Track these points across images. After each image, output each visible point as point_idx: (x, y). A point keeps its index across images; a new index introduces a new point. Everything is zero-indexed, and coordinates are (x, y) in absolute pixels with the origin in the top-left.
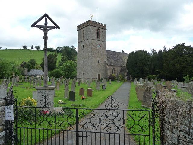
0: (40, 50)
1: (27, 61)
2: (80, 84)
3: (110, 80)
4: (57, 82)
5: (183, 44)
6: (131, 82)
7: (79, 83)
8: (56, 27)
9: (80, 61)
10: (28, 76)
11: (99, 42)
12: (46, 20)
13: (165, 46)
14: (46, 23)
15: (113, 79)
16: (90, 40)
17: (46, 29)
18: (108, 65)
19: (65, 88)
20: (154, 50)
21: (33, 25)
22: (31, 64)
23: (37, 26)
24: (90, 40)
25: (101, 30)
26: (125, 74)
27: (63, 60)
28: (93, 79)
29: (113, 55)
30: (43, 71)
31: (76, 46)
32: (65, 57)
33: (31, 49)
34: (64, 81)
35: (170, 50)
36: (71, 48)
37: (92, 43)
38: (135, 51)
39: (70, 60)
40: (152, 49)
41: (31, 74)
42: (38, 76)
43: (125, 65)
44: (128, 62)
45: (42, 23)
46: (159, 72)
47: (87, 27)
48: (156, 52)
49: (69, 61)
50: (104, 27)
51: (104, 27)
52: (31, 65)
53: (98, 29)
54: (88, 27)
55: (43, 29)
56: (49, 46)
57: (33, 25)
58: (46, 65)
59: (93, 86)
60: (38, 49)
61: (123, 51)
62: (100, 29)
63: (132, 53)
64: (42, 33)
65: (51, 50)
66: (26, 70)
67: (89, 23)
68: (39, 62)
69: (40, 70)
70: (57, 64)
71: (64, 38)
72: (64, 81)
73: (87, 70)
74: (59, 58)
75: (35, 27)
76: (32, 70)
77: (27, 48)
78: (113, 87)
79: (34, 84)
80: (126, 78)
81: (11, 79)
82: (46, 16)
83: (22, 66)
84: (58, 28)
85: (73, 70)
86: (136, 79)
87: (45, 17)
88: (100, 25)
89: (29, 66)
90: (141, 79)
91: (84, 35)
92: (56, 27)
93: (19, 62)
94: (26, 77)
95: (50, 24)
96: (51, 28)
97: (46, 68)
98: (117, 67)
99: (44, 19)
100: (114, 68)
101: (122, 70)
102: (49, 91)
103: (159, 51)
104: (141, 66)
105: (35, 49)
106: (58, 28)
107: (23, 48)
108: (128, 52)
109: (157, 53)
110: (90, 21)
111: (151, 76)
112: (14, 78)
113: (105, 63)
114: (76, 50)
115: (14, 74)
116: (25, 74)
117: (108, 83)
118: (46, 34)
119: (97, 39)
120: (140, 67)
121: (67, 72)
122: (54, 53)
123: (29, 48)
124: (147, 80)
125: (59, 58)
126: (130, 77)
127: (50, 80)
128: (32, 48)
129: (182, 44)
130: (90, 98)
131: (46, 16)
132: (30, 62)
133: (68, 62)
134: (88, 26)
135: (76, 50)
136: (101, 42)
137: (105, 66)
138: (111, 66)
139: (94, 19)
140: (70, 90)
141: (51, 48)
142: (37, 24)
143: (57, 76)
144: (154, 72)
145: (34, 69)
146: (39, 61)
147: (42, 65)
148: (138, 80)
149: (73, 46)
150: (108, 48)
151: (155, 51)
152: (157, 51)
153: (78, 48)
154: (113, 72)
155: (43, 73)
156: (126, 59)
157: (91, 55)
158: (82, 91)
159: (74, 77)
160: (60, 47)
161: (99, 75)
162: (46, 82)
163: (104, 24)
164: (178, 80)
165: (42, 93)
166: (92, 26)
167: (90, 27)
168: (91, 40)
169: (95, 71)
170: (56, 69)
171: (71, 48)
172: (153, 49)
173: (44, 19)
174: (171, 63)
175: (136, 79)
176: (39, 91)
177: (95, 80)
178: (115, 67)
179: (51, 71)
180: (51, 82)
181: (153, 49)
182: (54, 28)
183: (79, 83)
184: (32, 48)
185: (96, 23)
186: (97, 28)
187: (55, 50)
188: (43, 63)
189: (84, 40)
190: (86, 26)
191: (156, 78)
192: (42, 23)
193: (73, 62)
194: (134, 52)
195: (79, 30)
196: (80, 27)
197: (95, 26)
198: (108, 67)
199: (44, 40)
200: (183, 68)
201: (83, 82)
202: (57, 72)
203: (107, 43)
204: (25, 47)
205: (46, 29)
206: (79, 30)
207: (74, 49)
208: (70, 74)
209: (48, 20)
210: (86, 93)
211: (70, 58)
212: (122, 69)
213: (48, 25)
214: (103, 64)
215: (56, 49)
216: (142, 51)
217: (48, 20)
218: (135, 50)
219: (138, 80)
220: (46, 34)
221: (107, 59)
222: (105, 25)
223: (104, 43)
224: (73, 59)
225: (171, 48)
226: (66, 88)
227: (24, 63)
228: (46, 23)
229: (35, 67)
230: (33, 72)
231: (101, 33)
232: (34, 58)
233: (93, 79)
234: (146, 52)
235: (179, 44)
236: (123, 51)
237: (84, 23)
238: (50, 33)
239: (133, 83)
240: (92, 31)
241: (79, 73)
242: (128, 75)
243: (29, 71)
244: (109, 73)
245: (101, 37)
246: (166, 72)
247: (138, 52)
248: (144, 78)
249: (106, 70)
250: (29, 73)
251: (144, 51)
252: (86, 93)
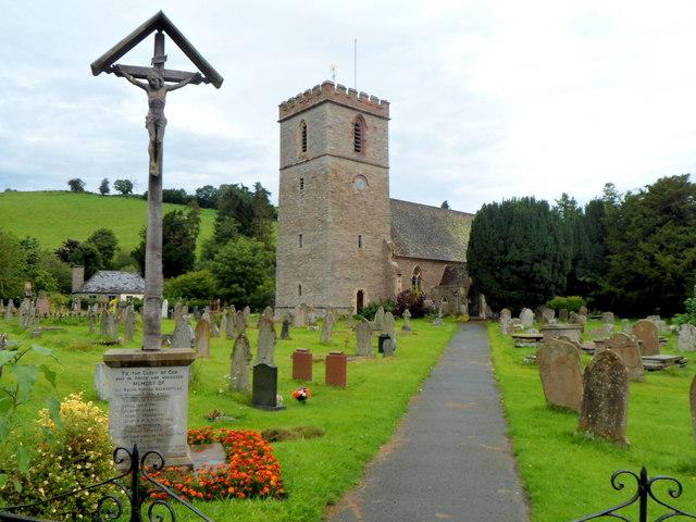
0: (136, 197)
1: (82, 238)
2: (290, 329)
3: (407, 313)
4: (201, 323)
5: (686, 177)
6: (483, 323)
7: (286, 326)
8: (203, 76)
9: (283, 238)
10: (87, 297)
11: (361, 169)
12: (159, 41)
13: (608, 185)
14: (159, 59)
15: (419, 312)
16: (328, 161)
17: (156, 82)
18: (396, 258)
19: (234, 349)
20: (570, 199)
21: (104, 65)
22: (100, 250)
23: (119, 72)
24: (328, 161)
25: (368, 120)
26: (462, 291)
27: (222, 238)
28: (339, 311)
29: (427, 221)
30: (143, 276)
31: (272, 185)
32: (231, 224)
33: (99, 192)
34: (224, 317)
35: (631, 200)
36: (252, 190)
37: (334, 171)
38: (499, 202)
39: (249, 235)
40: (559, 198)
41: (98, 287)
42: (123, 297)
43: (459, 255)
44: (471, 244)
45: (141, 56)
46: (595, 286)
47: (315, 110)
48: (578, 206)
49: (242, 241)
50: (380, 111)
51: (380, 111)
52: (94, 256)
53: (360, 118)
54: (320, 108)
55: (145, 82)
56: (169, 182)
57: (104, 65)
58: (154, 248)
59: (343, 338)
60: (125, 193)
61: (445, 205)
62: (365, 116)
63: (489, 212)
64: (139, 99)
65: (174, 197)
66: (78, 273)
67: (323, 97)
68: (129, 244)
69: (131, 272)
70: (198, 252)
71: (227, 141)
72: (224, 317)
73: (319, 278)
74: (207, 226)
75: (108, 72)
76: (102, 273)
77: (86, 189)
78: (419, 341)
79: (105, 325)
80: (464, 308)
81: (17, 304)
82: (160, 24)
83: (63, 256)
84: (213, 78)
85: (259, 276)
86: (506, 313)
87: (156, 31)
88: (367, 103)
89: (93, 255)
90: (528, 313)
91: (305, 140)
92: (203, 76)
93: (50, 243)
94: (77, 298)
95: (177, 61)
96: (181, 79)
97: (154, 262)
98: (429, 264)
99: (152, 37)
100: (417, 270)
101: (448, 278)
102: (167, 369)
103: (593, 203)
104: (519, 262)
105: (113, 191)
106: (213, 78)
107: (69, 188)
108: (469, 202)
109: (580, 209)
110: (328, 85)
111: (563, 300)
112: (26, 304)
113: (387, 248)
114: (274, 200)
115: (28, 286)
116: (74, 290)
117: (400, 323)
118: (156, 106)
119: (355, 156)
120: (520, 263)
121: (235, 286)
122: (186, 211)
123: (92, 187)
124: (549, 314)
125: (207, 226)
126: (479, 302)
127: (169, 314)
128: (104, 188)
129: (679, 174)
130: (333, 391)
131: (160, 24)
132: (94, 239)
133: (242, 245)
134: (320, 104)
135: (269, 198)
136: (368, 167)
137: (385, 261)
138: (405, 262)
139: (345, 79)
140: (254, 362)
141: (178, 188)
142: (122, 61)
143: (197, 297)
144: (574, 287)
145: (109, 268)
146: (127, 242)
147: (139, 258)
148: (516, 314)
149: (258, 185)
150: (393, 195)
151: (573, 202)
152: (582, 203)
153: (282, 190)
154: (414, 283)
155: (142, 283)
156: (463, 236)
157: (330, 219)
158: (302, 362)
159: (262, 303)
160: (208, 188)
161: (360, 295)
162: (152, 328)
163: (381, 97)
164: (667, 314)
165: (132, 380)
166: (336, 106)
167: (328, 106)
168: (334, 160)
169: (347, 279)
170: (192, 269)
171: (252, 190)
172: (565, 196)
173: (152, 37)
174: (640, 250)
175: (506, 313)
176: (119, 372)
177: (346, 312)
178: (423, 266)
179: (175, 276)
180: (177, 326)
181: (565, 196)
182: (196, 80)
183: (286, 326)
184: (104, 188)
185: (353, 92)
186: (355, 114)
187: (190, 199)
188: (143, 245)
189: (303, 157)
190: (314, 107)
191: (584, 309)
192: (141, 56)
193: (261, 244)
194: (495, 205)
195: (285, 120)
196: (292, 111)
197: (348, 107)
198: (395, 264)
199: (151, 135)
200: (685, 271)
201: (299, 320)
202: (199, 281)
203: (392, 172)
204: (76, 185)
205: (156, 82)
206: (285, 120)
207: (262, 194)
208: (244, 290)
209: (169, 42)
210: (319, 372)
211: (247, 230)
212: (447, 270)
213: (168, 66)
214: (377, 251)
215: (194, 194)
216: (528, 203)
217: (170, 45)
218: (498, 196)
219: (516, 314)
220: (156, 106)
221: (393, 235)
222: (386, 103)
223: (382, 170)
224: (260, 234)
225: (636, 193)
226: (240, 348)
227: (72, 244)
228: (159, 59)
229: (114, 260)
230: (104, 280)
231: (368, 134)
232: (109, 228)
233: (339, 311)
234: (544, 204)
235: (669, 175)
236: (445, 205)
237: (306, 93)
238: (181, 105)
239: (493, 328)
240: (334, 124)
241: (285, 289)
242: (472, 294)
243: (87, 277)
244: (399, 286)
245: (369, 150)
246: (619, 287)
247: (508, 206)
248: (535, 305)
249: (388, 277)
250: (90, 284)
251: (538, 199)
252: (319, 372)
